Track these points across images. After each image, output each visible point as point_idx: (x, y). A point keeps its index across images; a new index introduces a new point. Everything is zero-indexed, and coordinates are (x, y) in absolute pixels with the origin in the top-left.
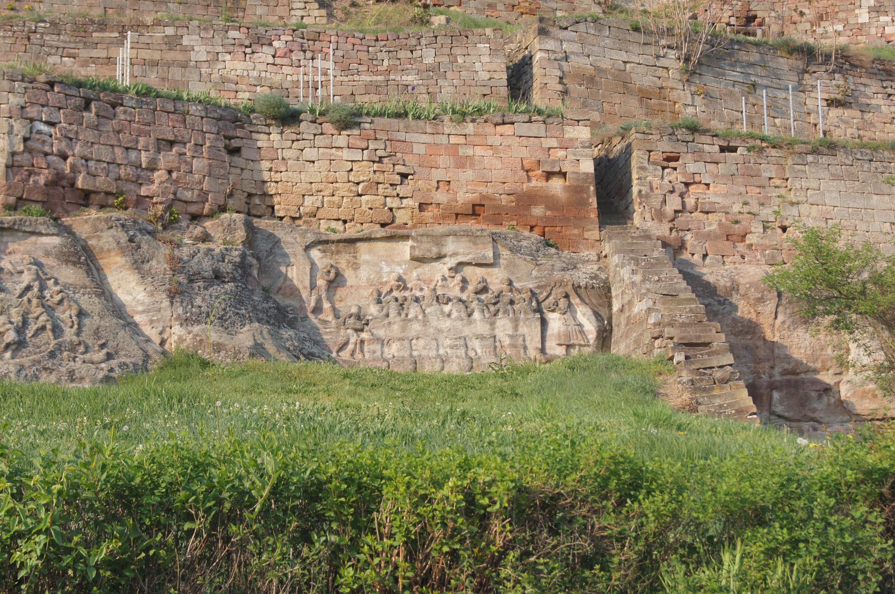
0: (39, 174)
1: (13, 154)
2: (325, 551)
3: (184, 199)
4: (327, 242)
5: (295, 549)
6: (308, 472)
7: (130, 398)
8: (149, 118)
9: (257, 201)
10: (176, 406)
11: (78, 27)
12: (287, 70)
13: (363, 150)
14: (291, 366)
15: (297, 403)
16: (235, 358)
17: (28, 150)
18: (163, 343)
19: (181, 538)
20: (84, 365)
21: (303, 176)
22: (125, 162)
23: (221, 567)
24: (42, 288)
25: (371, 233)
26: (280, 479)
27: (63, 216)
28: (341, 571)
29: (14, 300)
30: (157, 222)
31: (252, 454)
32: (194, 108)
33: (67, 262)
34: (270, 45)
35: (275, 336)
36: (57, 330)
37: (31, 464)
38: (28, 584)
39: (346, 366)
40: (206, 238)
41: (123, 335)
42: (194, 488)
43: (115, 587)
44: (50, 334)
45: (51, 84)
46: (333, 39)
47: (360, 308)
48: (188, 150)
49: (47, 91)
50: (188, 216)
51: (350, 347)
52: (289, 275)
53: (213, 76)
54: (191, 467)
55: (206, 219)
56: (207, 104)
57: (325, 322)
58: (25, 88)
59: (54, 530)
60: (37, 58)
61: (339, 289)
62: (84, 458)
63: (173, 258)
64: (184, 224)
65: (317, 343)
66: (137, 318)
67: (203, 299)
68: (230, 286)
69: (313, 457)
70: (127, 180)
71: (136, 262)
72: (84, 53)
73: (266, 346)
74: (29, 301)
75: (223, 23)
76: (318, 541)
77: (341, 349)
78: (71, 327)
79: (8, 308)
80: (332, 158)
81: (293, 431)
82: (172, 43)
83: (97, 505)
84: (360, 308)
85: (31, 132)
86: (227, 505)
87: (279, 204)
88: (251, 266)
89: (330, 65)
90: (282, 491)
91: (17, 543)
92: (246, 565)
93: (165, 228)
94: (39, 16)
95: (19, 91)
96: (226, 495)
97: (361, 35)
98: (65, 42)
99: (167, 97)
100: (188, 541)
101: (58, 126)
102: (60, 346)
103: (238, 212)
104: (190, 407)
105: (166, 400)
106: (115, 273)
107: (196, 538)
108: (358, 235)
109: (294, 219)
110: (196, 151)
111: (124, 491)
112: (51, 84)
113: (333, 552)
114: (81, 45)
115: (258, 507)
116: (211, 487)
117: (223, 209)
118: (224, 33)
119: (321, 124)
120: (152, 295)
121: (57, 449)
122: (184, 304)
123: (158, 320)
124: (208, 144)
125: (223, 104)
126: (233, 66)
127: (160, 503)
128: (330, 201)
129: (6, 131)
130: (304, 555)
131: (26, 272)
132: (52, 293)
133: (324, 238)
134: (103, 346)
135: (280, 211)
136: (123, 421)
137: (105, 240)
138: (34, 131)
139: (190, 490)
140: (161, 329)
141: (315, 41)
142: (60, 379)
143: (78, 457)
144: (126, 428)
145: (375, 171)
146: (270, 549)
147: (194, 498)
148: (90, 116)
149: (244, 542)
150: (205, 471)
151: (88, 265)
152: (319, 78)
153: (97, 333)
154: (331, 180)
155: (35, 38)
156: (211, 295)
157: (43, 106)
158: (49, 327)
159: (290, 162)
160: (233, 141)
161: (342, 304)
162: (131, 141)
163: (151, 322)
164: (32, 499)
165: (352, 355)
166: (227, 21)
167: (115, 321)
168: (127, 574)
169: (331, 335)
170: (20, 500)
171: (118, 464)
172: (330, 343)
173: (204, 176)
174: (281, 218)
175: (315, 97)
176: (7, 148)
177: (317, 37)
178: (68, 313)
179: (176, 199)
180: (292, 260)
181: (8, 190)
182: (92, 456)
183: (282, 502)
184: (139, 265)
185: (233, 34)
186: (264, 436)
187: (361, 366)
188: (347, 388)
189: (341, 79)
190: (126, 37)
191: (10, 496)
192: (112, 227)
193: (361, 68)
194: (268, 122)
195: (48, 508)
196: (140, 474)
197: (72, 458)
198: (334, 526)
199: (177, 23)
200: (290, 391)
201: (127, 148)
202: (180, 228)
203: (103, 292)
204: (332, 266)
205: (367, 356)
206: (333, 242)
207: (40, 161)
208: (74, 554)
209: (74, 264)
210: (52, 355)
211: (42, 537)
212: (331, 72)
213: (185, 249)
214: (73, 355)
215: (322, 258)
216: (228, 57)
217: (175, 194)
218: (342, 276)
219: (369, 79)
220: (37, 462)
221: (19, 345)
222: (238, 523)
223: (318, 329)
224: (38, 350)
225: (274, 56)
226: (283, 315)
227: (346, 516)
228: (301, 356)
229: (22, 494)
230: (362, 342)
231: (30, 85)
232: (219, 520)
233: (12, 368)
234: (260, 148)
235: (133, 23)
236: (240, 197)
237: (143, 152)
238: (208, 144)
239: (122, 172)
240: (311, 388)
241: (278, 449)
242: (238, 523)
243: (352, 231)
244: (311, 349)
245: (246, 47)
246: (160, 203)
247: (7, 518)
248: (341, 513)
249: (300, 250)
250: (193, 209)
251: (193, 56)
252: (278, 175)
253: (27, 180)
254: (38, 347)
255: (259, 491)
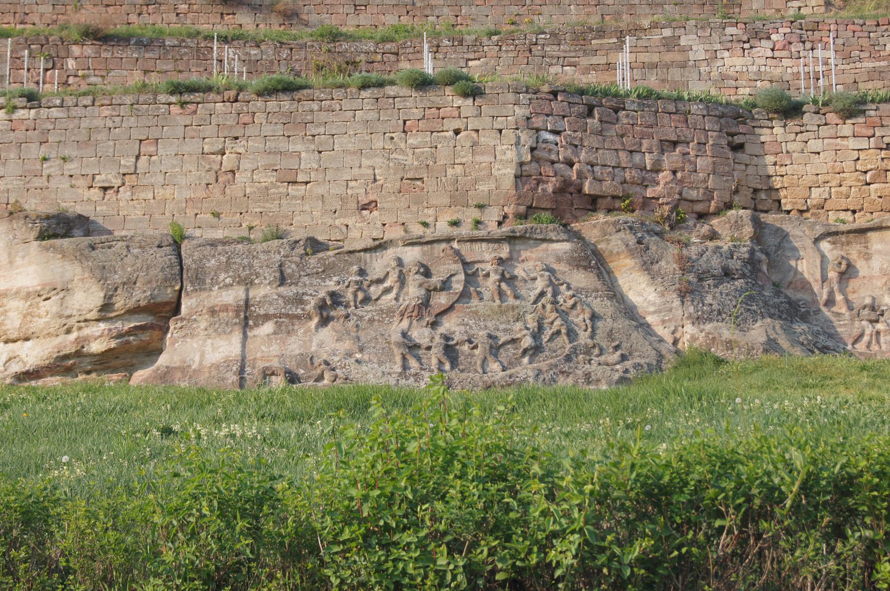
0: (547, 182)
1: (521, 164)
2: (859, 547)
3: (689, 198)
4: (836, 233)
5: (828, 545)
6: (838, 467)
7: (649, 398)
8: (651, 120)
9: (763, 196)
10: (696, 405)
11: (577, 36)
12: (786, 62)
13: (869, 138)
14: (806, 361)
15: (819, 397)
16: (748, 354)
17: (535, 159)
18: (675, 342)
19: (712, 535)
20: (599, 367)
21: (808, 167)
22: (630, 165)
23: (754, 564)
24: (555, 294)
25: (881, 222)
26: (809, 474)
27: (572, 222)
28: (878, 566)
29: (529, 306)
30: (664, 222)
31: (779, 450)
32: (695, 107)
33: (578, 267)
34: (769, 38)
35: (788, 331)
36: (572, 334)
37: (559, 465)
38: (565, 583)
39: (863, 358)
40: (713, 236)
41: (636, 336)
42: (723, 485)
43: (649, 585)
44: (565, 338)
45: (555, 94)
46: (832, 27)
47: (874, 298)
48: (692, 149)
49: (551, 101)
50: (694, 215)
51: (866, 338)
52: (800, 269)
53: (712, 74)
54: (719, 464)
55: (712, 217)
56: (708, 102)
57: (838, 314)
58: (530, 99)
59: (588, 530)
60: (540, 69)
61: (851, 281)
62: (613, 459)
63: (682, 258)
64: (691, 223)
65: (831, 336)
66: (649, 319)
67: (714, 297)
68: (740, 283)
69: (842, 451)
70: (633, 183)
71: (645, 263)
72: (584, 61)
73: (779, 342)
74: (544, 306)
75: (720, 20)
76: (853, 536)
77: (856, 341)
78: (586, 330)
79: (524, 315)
80: (838, 148)
81: (816, 426)
82: (670, 44)
83: (628, 503)
84: (874, 298)
85: (537, 142)
86: (757, 502)
87: (786, 197)
88: (760, 262)
89: (832, 54)
90: (812, 486)
91: (552, 543)
92: (779, 562)
93: (672, 228)
94: (539, 28)
95: (524, 102)
96: (755, 491)
97: (861, 22)
98: (565, 51)
99: (669, 98)
100: (719, 539)
101: (563, 134)
102: (576, 349)
103: (744, 208)
104: (709, 404)
105: (686, 398)
106: (625, 275)
107: (727, 534)
108: (868, 225)
109: (801, 212)
110: (700, 150)
111: (653, 490)
112: (555, 94)
113: (868, 547)
114: (581, 54)
115: (788, 503)
116: (740, 484)
117: (729, 206)
118: (721, 30)
119: (824, 114)
120: (663, 295)
121: (586, 451)
122: (695, 303)
123: (670, 320)
124: (711, 142)
125: (724, 101)
126: (733, 62)
127: (690, 501)
128: (837, 192)
129: (513, 143)
130: (838, 550)
131: (539, 279)
132: (565, 298)
133: (833, 229)
134: (617, 348)
135: (787, 205)
136: (645, 421)
137: (613, 243)
138: (540, 141)
139: (719, 487)
140: (673, 328)
141: (814, 31)
142: (577, 382)
143: (607, 457)
144: (648, 427)
145: (882, 159)
146: (803, 545)
147: (723, 495)
148: (593, 122)
149: (776, 538)
150: (733, 468)
151: (599, 268)
152: (820, 68)
153: (610, 335)
154: (837, 170)
155: (537, 50)
156: (721, 293)
157: (547, 115)
158: (563, 331)
159: (794, 155)
160: (735, 137)
161: (855, 295)
162: (634, 145)
163: (663, 322)
164: (564, 500)
165: (868, 347)
166: (724, 18)
167: (627, 322)
168: (661, 571)
169: (845, 328)
170: (553, 500)
171: (646, 463)
172: (845, 336)
173: (709, 174)
174: (788, 212)
175: (817, 88)
176: (515, 159)
177: (816, 26)
178: (581, 317)
179: (682, 199)
180: (802, 253)
181: (518, 199)
182: (620, 455)
183: (812, 497)
184: (648, 266)
185: (730, 30)
186: (791, 432)
187: (879, 357)
188: (865, 380)
189: (843, 67)
190: (624, 42)
191: (543, 498)
192: (620, 230)
193: (863, 55)
194: (771, 116)
195: (580, 507)
196: (668, 472)
197: (600, 458)
198: (868, 520)
199: (674, 24)
200: (806, 386)
201: (631, 152)
202: (687, 228)
203: (615, 294)
204: (843, 258)
205: (884, 347)
206: (843, 233)
207: (547, 169)
208: (608, 553)
209: (585, 268)
210: (568, 359)
211: (577, 536)
212: (832, 61)
213: (693, 248)
214: (588, 358)
215: (832, 250)
216: (726, 54)
217: (680, 194)
218: (854, 267)
219: (871, 65)
220: (567, 463)
221: (536, 350)
222: (769, 519)
223: (831, 322)
224: (554, 354)
225: (773, 50)
226: (793, 308)
227: (878, 510)
228: (816, 350)
229: (554, 495)
230: (878, 333)
231: (535, 96)
232: (750, 517)
233: (530, 373)
234: (763, 143)
235: (631, 27)
236: (746, 193)
237: (647, 154)
238: (711, 142)
239: (627, 175)
240: (828, 382)
241: (806, 442)
242: (769, 519)
243: (861, 221)
244: (826, 342)
245: (744, 42)
246: (666, 204)
247: (542, 519)
248: (874, 507)
249: (809, 243)
250: (699, 207)
251: (692, 56)
252: (783, 168)
253: (536, 189)
254: (554, 352)
255: (788, 486)
